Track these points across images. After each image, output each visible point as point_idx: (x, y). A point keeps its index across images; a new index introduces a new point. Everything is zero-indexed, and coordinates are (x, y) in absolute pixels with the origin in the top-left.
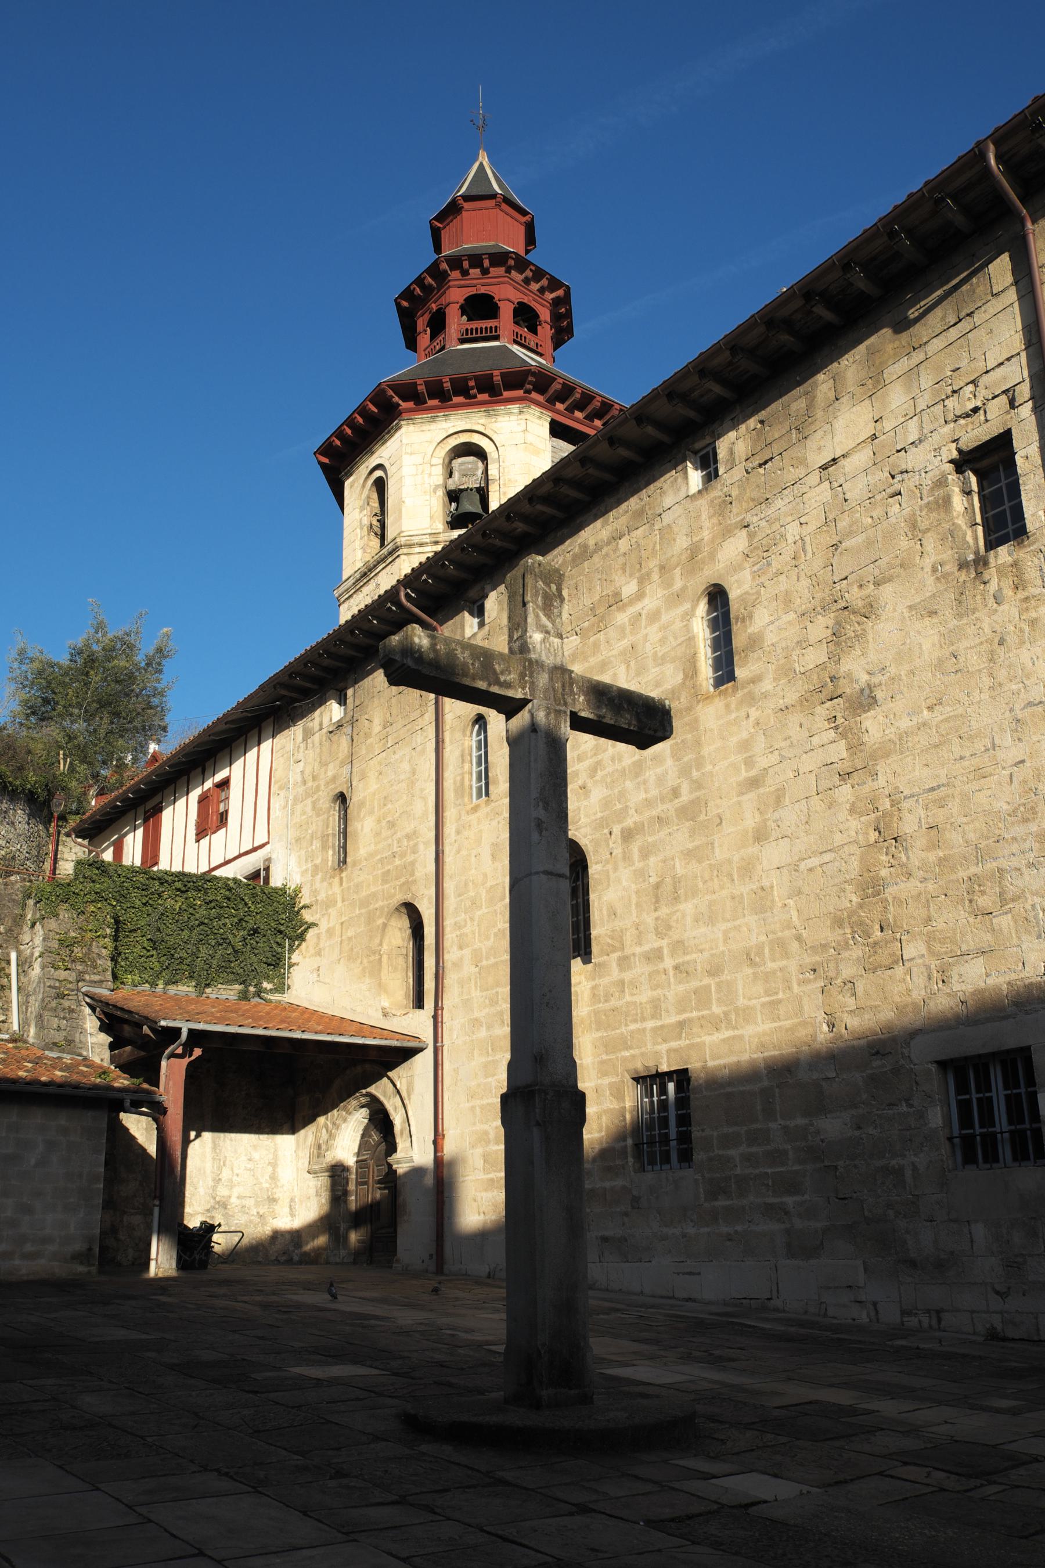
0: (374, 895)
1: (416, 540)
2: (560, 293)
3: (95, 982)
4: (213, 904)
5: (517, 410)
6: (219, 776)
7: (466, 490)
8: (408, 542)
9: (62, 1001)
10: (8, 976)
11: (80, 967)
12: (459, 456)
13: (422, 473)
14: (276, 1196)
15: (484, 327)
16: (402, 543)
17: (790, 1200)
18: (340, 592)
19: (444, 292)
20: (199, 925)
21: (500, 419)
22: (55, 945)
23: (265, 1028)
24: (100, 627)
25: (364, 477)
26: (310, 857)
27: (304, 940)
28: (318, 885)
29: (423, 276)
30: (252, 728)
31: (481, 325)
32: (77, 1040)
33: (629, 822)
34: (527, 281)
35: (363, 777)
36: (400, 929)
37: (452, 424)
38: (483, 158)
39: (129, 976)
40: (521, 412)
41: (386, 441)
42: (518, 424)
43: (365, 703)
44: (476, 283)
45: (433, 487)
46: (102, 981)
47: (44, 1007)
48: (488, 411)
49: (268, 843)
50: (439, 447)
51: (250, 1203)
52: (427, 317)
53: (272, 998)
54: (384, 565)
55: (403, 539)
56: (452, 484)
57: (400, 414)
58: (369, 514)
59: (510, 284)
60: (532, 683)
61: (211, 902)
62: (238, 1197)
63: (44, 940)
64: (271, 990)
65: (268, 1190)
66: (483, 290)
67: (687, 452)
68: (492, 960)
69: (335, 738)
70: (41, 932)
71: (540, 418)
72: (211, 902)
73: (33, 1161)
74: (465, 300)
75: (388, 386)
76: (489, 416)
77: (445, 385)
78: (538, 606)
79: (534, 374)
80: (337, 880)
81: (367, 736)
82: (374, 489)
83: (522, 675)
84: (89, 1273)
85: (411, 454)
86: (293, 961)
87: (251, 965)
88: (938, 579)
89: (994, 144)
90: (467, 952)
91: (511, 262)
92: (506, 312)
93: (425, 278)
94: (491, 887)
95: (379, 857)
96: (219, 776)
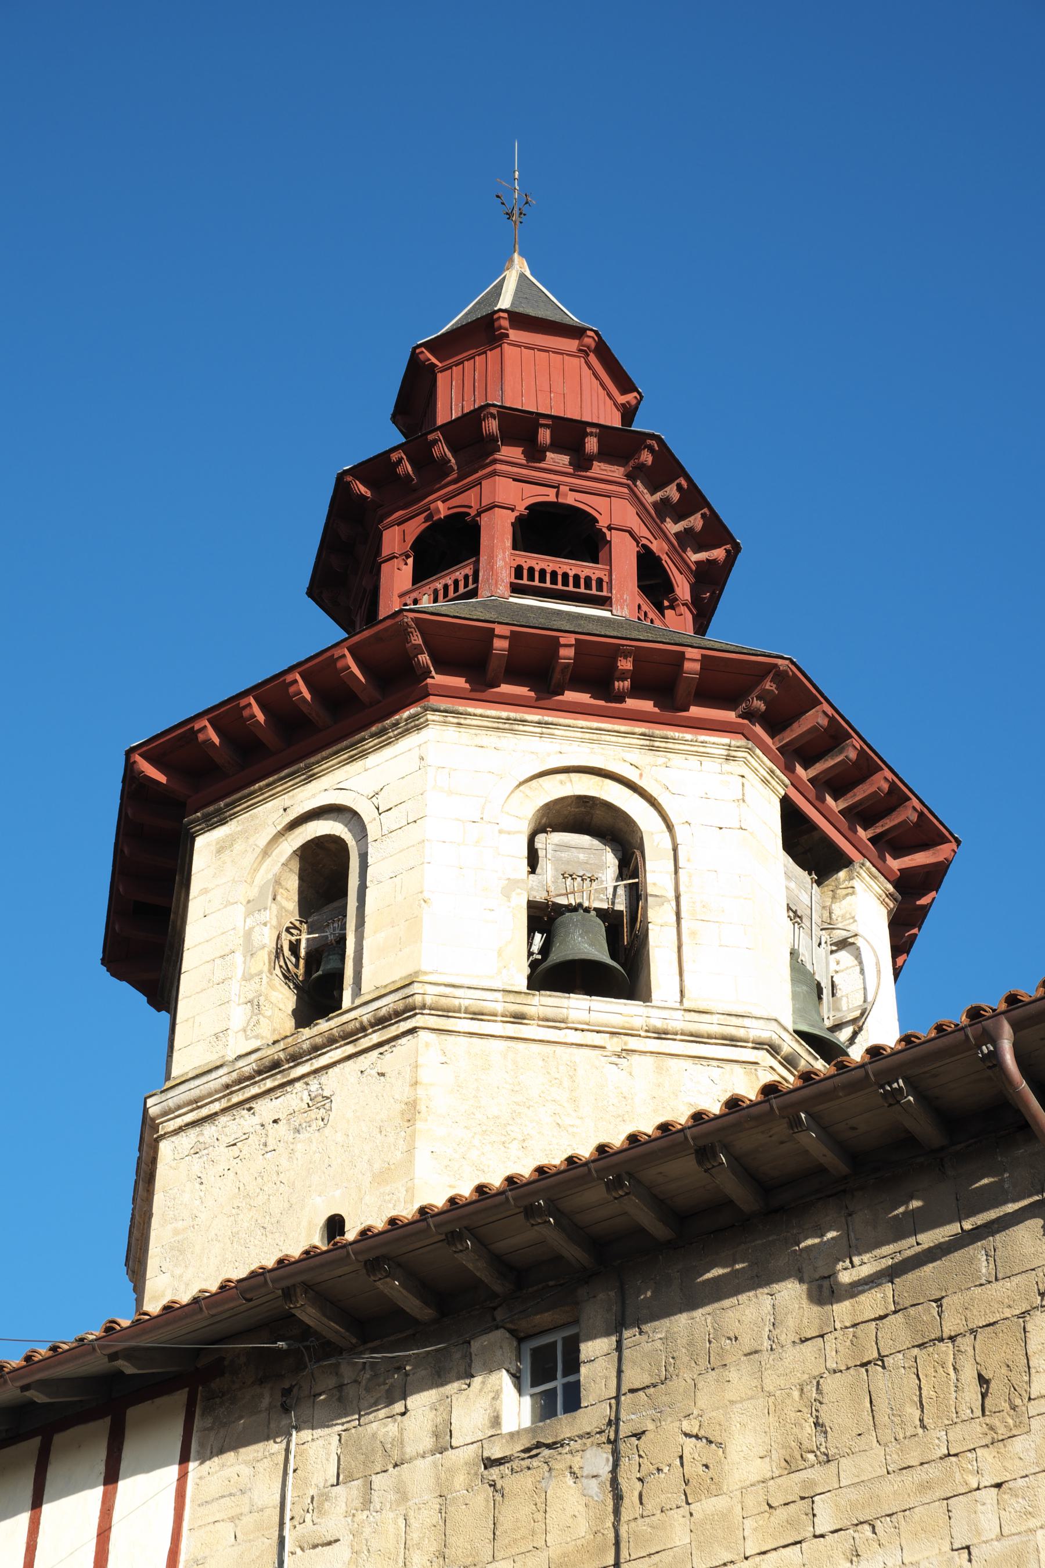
1: (466, 999)
8: (444, 1002)
12: (556, 829)
16: (429, 1000)
18: (171, 1103)
19: (478, 483)
21: (676, 760)
31: (566, 569)
34: (664, 509)
41: (364, 754)
43: (677, 1385)
48: (650, 737)
52: (416, 527)
54: (350, 1049)
57: (426, 695)
66: (570, 499)
76: (652, 749)
82: (295, 865)
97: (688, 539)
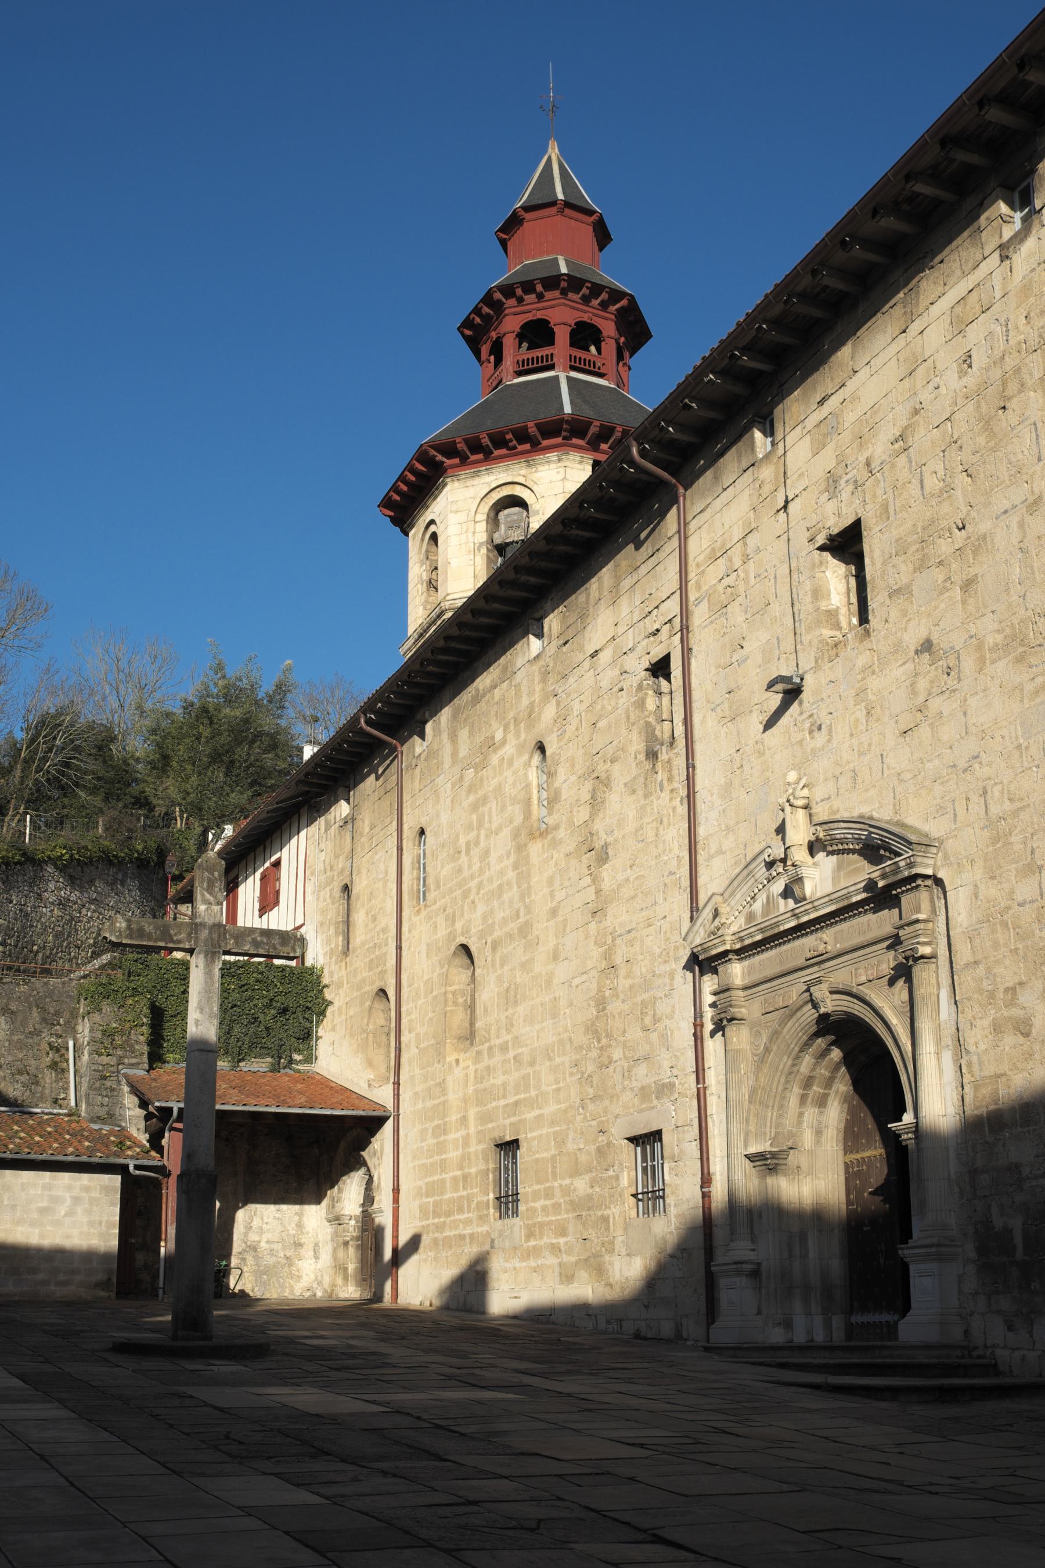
0: (364, 980)
2: (624, 302)
3: (133, 1065)
4: (246, 987)
5: (556, 458)
6: (273, 859)
7: (512, 543)
9: (105, 1082)
10: (67, 1061)
11: (119, 1053)
12: (506, 508)
13: (466, 532)
14: (302, 1241)
15: (540, 355)
16: (447, 607)
17: (562, 1241)
20: (232, 1008)
21: (541, 468)
22: (99, 1035)
23: (244, 1105)
24: (220, 668)
25: (422, 530)
26: (328, 941)
27: (325, 1016)
28: (333, 968)
29: (479, 306)
30: (285, 822)
32: (117, 1114)
33: (497, 934)
34: (586, 300)
35: (359, 873)
36: (383, 1011)
37: (495, 477)
38: (553, 152)
39: (171, 1055)
40: (560, 460)
42: (558, 472)
44: (532, 309)
45: (476, 546)
46: (139, 1064)
47: (90, 1088)
49: (303, 925)
50: (483, 503)
51: (277, 1247)
53: (300, 1068)
55: (447, 603)
56: (498, 539)
58: (428, 568)
59: (565, 305)
60: (196, 938)
61: (244, 985)
62: (267, 1242)
63: (90, 1031)
64: (300, 1061)
65: (294, 1236)
66: (539, 315)
67: (530, 621)
68: (426, 1044)
69: (343, 833)
70: (88, 1025)
71: (580, 462)
72: (244, 985)
73: (63, 1212)
74: (521, 328)
75: (429, 446)
77: (482, 441)
78: (204, 889)
79: (567, 422)
80: (343, 964)
81: (362, 835)
83: (189, 934)
84: (109, 1297)
85: (456, 512)
86: (319, 1034)
87: (281, 1040)
88: (637, 764)
89: (635, 440)
90: (413, 1035)
91: (564, 284)
92: (562, 336)
93: (481, 308)
94: (427, 980)
95: (367, 947)
96: (273, 859)
97: (604, 305)
